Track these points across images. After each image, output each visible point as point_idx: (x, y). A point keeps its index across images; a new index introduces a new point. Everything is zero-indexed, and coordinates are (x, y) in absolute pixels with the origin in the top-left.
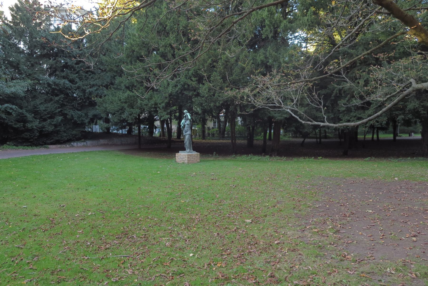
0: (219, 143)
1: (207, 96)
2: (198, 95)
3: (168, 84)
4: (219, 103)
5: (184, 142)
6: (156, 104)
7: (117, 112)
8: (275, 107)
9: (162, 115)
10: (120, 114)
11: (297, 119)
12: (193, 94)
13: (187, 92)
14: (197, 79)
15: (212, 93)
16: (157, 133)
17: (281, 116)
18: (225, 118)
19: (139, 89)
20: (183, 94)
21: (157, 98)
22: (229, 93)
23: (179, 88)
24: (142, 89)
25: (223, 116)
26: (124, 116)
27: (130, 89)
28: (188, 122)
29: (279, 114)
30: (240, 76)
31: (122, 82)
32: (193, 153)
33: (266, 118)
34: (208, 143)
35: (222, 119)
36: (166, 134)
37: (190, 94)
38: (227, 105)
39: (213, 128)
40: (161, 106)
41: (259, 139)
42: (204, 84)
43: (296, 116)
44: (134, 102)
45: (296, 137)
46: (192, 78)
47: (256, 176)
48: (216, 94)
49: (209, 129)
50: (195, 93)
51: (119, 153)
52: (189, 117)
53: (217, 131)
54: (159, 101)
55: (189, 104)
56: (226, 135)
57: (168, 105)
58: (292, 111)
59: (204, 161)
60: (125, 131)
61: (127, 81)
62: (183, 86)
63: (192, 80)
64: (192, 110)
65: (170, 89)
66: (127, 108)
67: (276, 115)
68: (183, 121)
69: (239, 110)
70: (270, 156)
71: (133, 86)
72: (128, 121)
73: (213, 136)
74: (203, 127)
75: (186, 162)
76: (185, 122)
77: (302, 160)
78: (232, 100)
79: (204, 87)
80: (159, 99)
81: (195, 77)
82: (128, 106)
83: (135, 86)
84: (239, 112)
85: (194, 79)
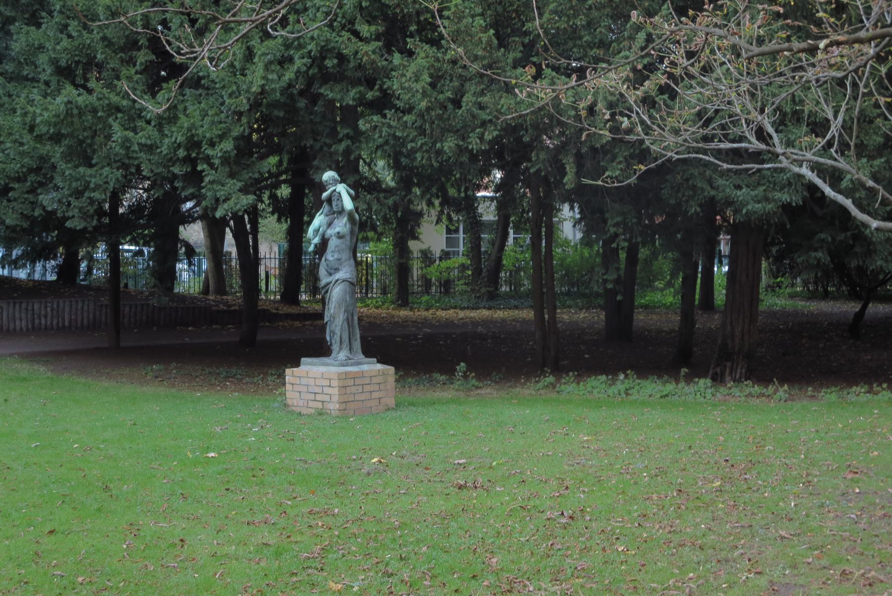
0: (475, 323)
1: (424, 104)
2: (383, 103)
3: (250, 55)
4: (481, 138)
5: (320, 316)
6: (193, 144)
7: (18, 180)
8: (737, 155)
9: (221, 194)
10: (32, 191)
11: (844, 210)
12: (361, 101)
13: (338, 88)
14: (381, 29)
15: (449, 94)
16: (188, 278)
17: (767, 199)
18: (499, 208)
19: (118, 78)
20: (314, 99)
21: (198, 117)
22: (535, 91)
23: (298, 71)
24: (129, 78)
25: (492, 199)
26: (48, 200)
27: (79, 81)
28: (341, 225)
29: (755, 188)
30: (575, 16)
31: (41, 47)
32: (365, 367)
33: (694, 209)
34: (425, 322)
35: (488, 213)
36: (236, 282)
37: (351, 96)
38: (510, 147)
39: (445, 256)
40: (216, 153)
41: (660, 300)
42: (410, 54)
43: (840, 198)
44: (95, 134)
45: (826, 296)
46: (357, 27)
47: (662, 472)
48: (468, 99)
49: (427, 257)
50: (370, 95)
51: (24, 369)
52: (348, 204)
53: (463, 267)
54: (206, 131)
55: (342, 147)
56: (504, 288)
57: (246, 150)
58: (816, 167)
59: (412, 404)
60: (46, 271)
61: (65, 43)
62: (318, 60)
63: (356, 34)
64: (357, 170)
65: (256, 77)
66: (62, 165)
67: (741, 194)
68: (319, 220)
69: (570, 169)
70: (714, 379)
71: (90, 63)
72: (68, 224)
73: (447, 292)
74: (401, 248)
75: (334, 406)
76: (330, 225)
77: (864, 398)
78: (547, 119)
79: (413, 68)
80: (207, 119)
81: (369, 23)
82: (67, 157)
83: (100, 66)
84: (569, 180)
85: (365, 29)
